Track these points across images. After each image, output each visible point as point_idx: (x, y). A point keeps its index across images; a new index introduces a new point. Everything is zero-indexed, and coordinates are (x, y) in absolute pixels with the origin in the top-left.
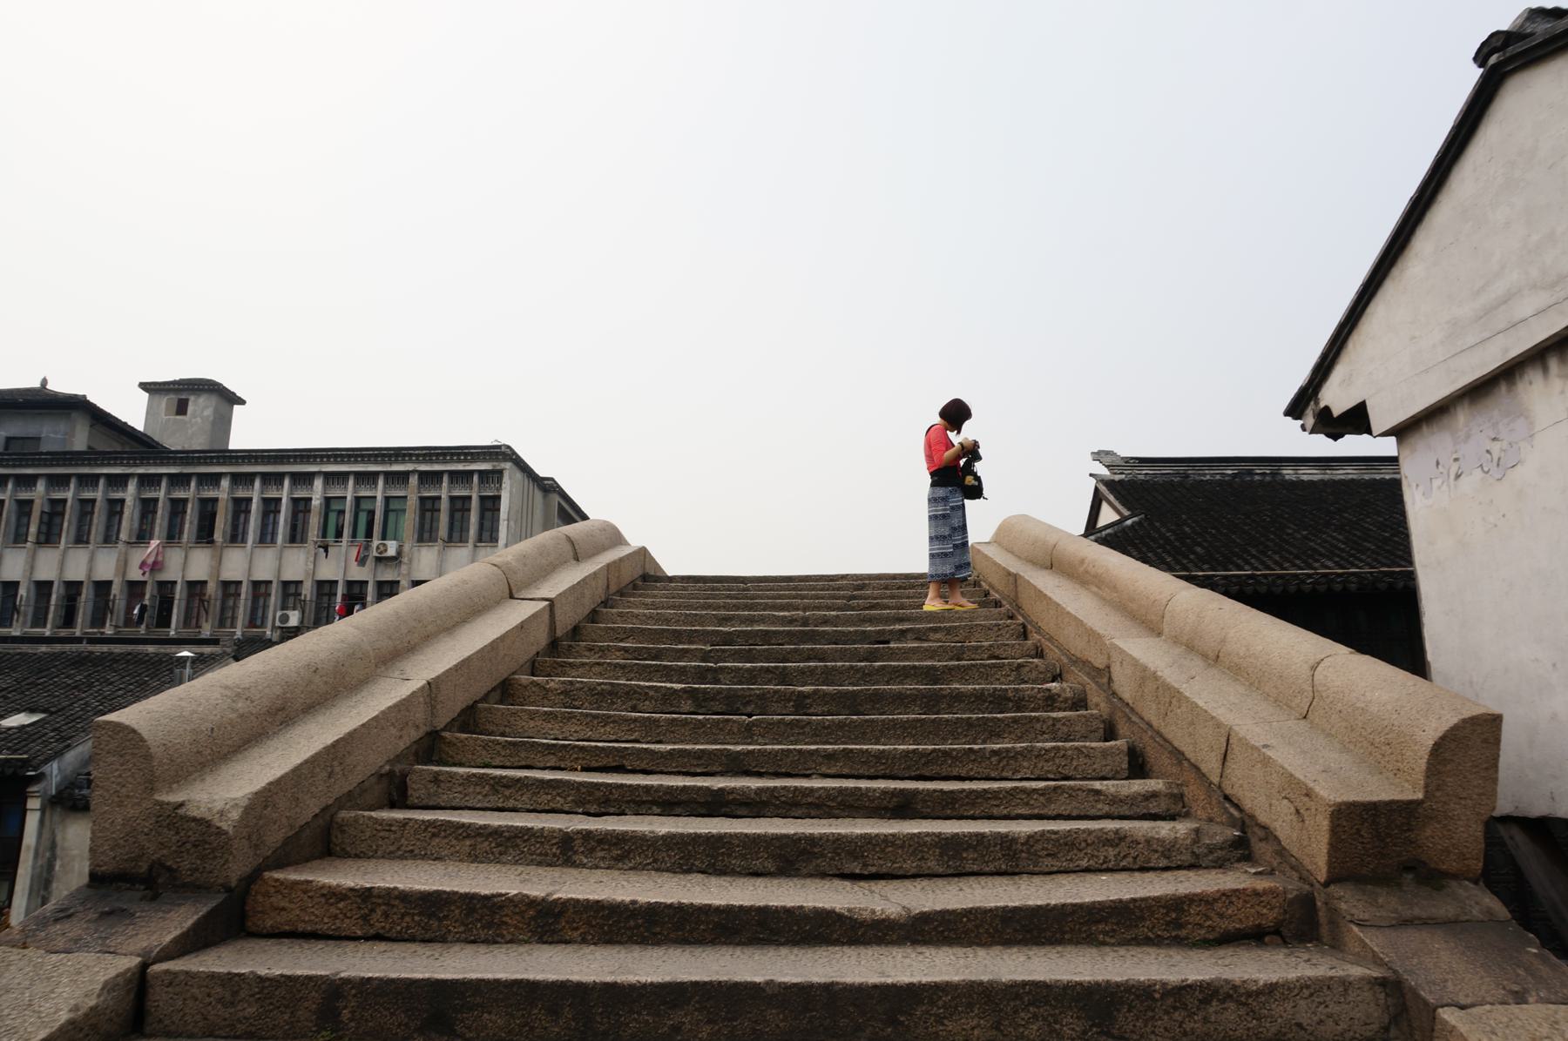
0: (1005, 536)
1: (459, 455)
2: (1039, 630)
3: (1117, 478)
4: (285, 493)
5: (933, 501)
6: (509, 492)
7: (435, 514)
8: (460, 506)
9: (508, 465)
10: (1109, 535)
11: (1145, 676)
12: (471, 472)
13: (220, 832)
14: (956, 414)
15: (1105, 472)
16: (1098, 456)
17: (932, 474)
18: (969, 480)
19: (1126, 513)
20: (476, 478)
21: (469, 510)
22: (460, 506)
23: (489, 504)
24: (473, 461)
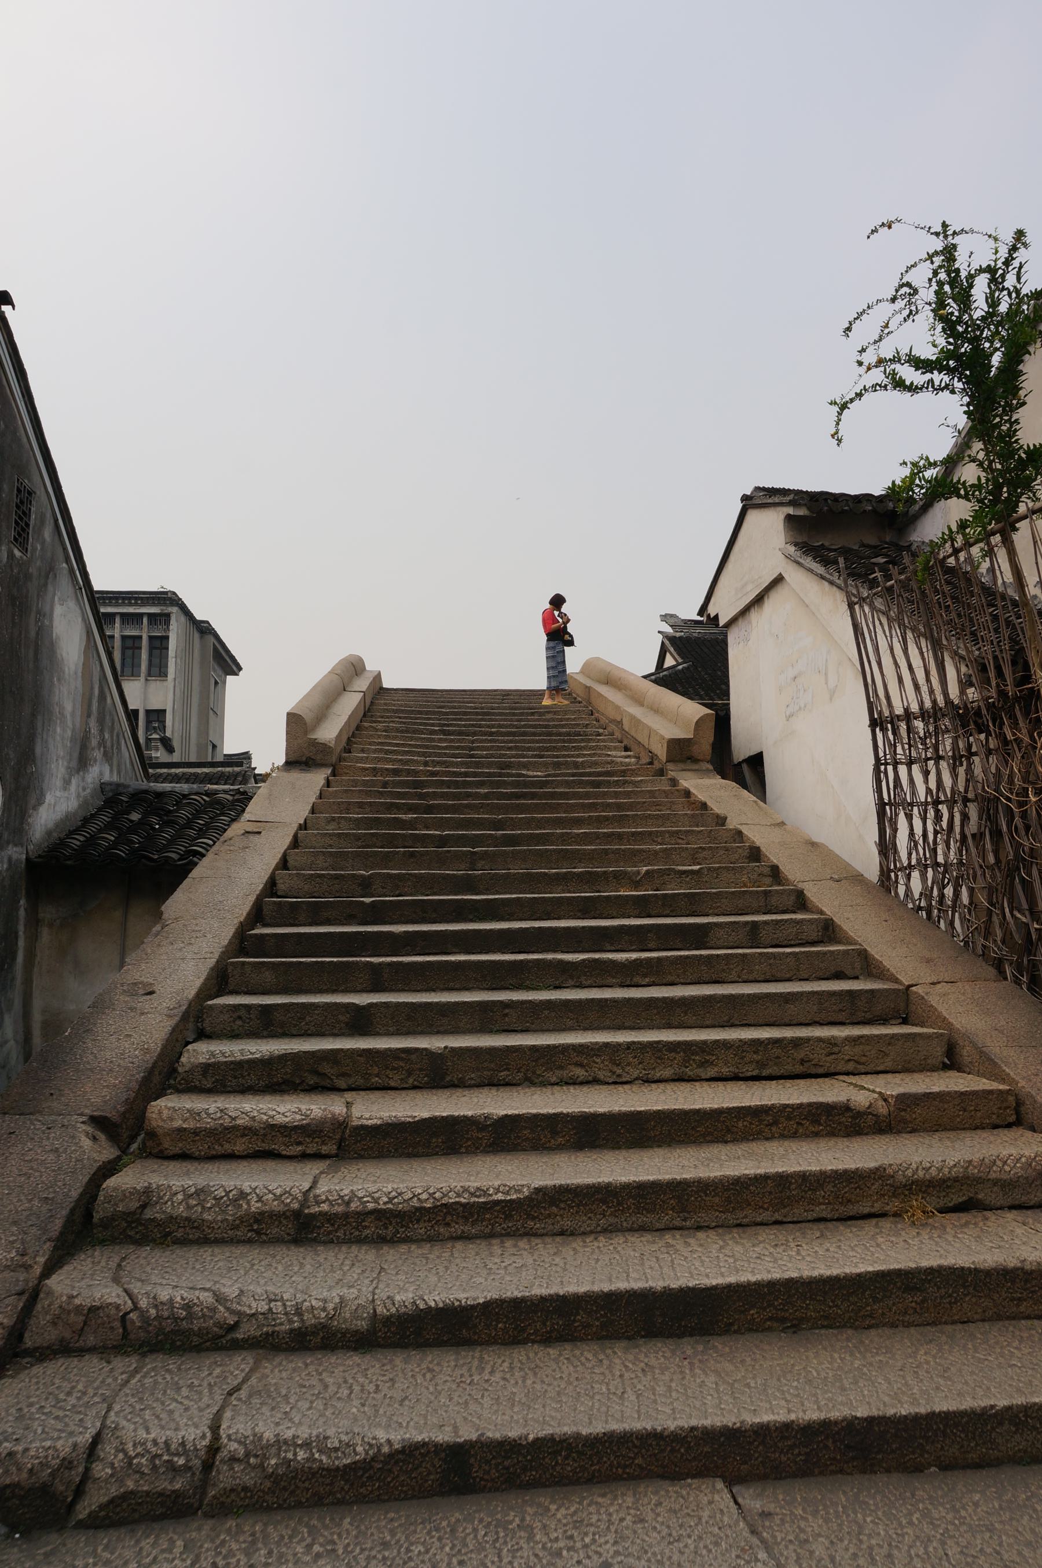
0: (588, 668)
1: (130, 599)
2: (598, 712)
3: (678, 635)
4: (144, 633)
5: (548, 649)
6: (175, 633)
7: (136, 651)
8: (131, 644)
9: (174, 610)
10: (665, 676)
11: (633, 718)
12: (141, 615)
13: (330, 747)
14: (558, 601)
15: (669, 630)
16: (665, 618)
17: (547, 635)
18: (567, 637)
19: (680, 660)
20: (145, 620)
21: (140, 648)
22: (131, 644)
23: (157, 643)
24: (143, 605)
